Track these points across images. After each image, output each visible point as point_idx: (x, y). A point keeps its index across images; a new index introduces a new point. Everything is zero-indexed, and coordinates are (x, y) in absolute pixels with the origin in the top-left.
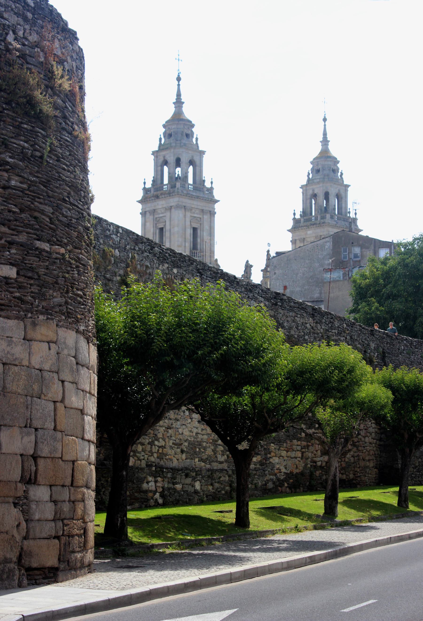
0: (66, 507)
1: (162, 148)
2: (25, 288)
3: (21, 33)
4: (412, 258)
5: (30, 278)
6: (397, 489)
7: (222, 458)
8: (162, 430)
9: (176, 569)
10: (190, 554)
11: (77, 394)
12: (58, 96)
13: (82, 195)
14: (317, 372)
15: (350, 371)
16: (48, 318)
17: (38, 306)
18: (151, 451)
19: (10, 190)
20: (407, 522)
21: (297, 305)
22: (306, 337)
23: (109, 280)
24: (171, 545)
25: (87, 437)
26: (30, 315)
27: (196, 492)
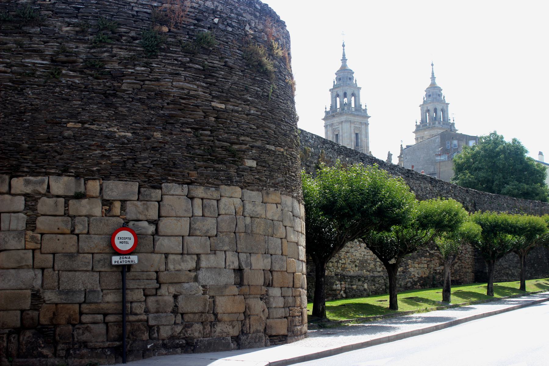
0: (290, 300)
1: (335, 87)
2: (261, 172)
3: (253, 25)
4: (489, 146)
5: (264, 167)
6: (486, 285)
7: (379, 269)
8: (343, 253)
9: (356, 335)
10: (363, 326)
11: (294, 234)
12: (276, 60)
13: (292, 117)
14: (435, 216)
15: (456, 215)
16: (275, 190)
17: (269, 183)
18: (337, 266)
19: (250, 116)
20: (493, 304)
21: (421, 177)
22: (427, 195)
23: (309, 166)
24: (352, 321)
25: (300, 259)
26: (265, 188)
27: (365, 290)
